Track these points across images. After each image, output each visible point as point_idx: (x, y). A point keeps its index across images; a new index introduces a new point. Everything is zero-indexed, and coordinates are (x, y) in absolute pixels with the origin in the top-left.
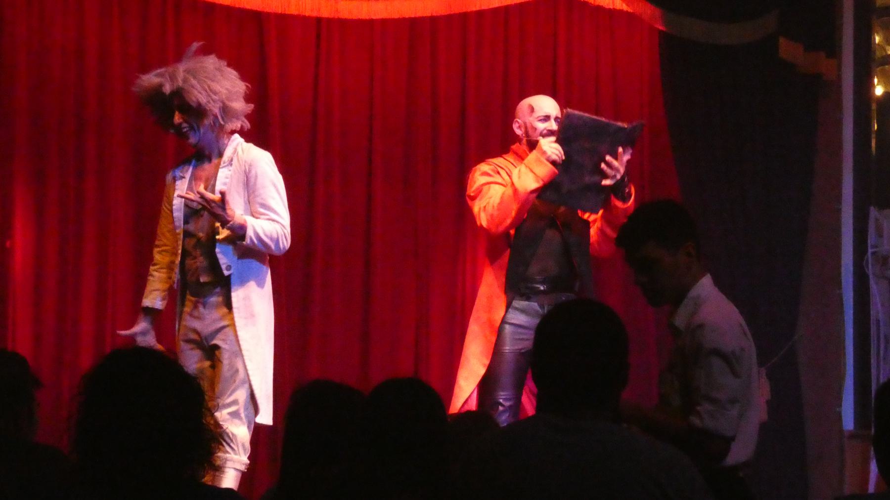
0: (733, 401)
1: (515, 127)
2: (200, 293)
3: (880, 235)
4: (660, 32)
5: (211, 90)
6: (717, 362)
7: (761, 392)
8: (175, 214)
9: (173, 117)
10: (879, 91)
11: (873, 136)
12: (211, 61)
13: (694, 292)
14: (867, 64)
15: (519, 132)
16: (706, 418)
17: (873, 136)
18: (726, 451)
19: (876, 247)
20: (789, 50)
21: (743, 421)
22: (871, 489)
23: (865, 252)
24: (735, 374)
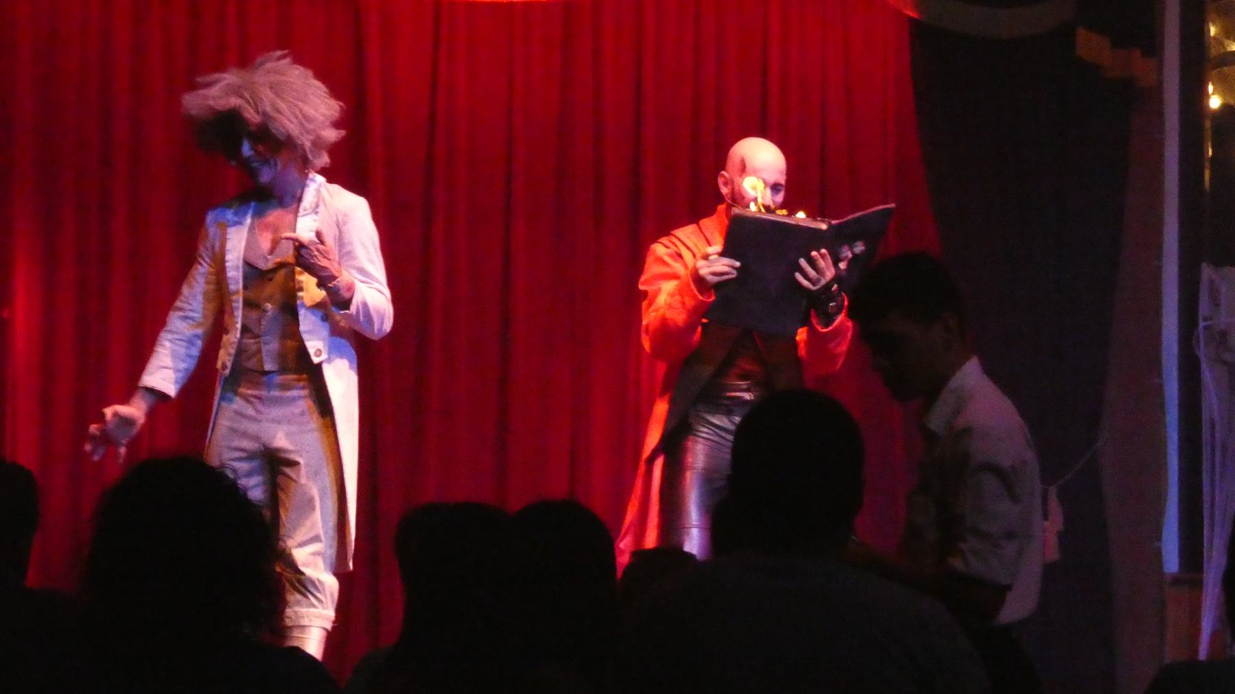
0: (1010, 535)
1: (720, 181)
2: (246, 374)
3: (1216, 305)
4: (911, 20)
5: (305, 116)
6: (990, 483)
7: (1047, 530)
8: (231, 273)
9: (240, 146)
10: (1215, 102)
11: (1207, 164)
12: (297, 72)
13: (954, 382)
14: (1198, 64)
15: (725, 190)
16: (971, 560)
17: (1207, 164)
18: (999, 603)
19: (1211, 319)
20: (1091, 46)
21: (1022, 554)
22: (1203, 654)
23: (1196, 324)
24: (1015, 499)
